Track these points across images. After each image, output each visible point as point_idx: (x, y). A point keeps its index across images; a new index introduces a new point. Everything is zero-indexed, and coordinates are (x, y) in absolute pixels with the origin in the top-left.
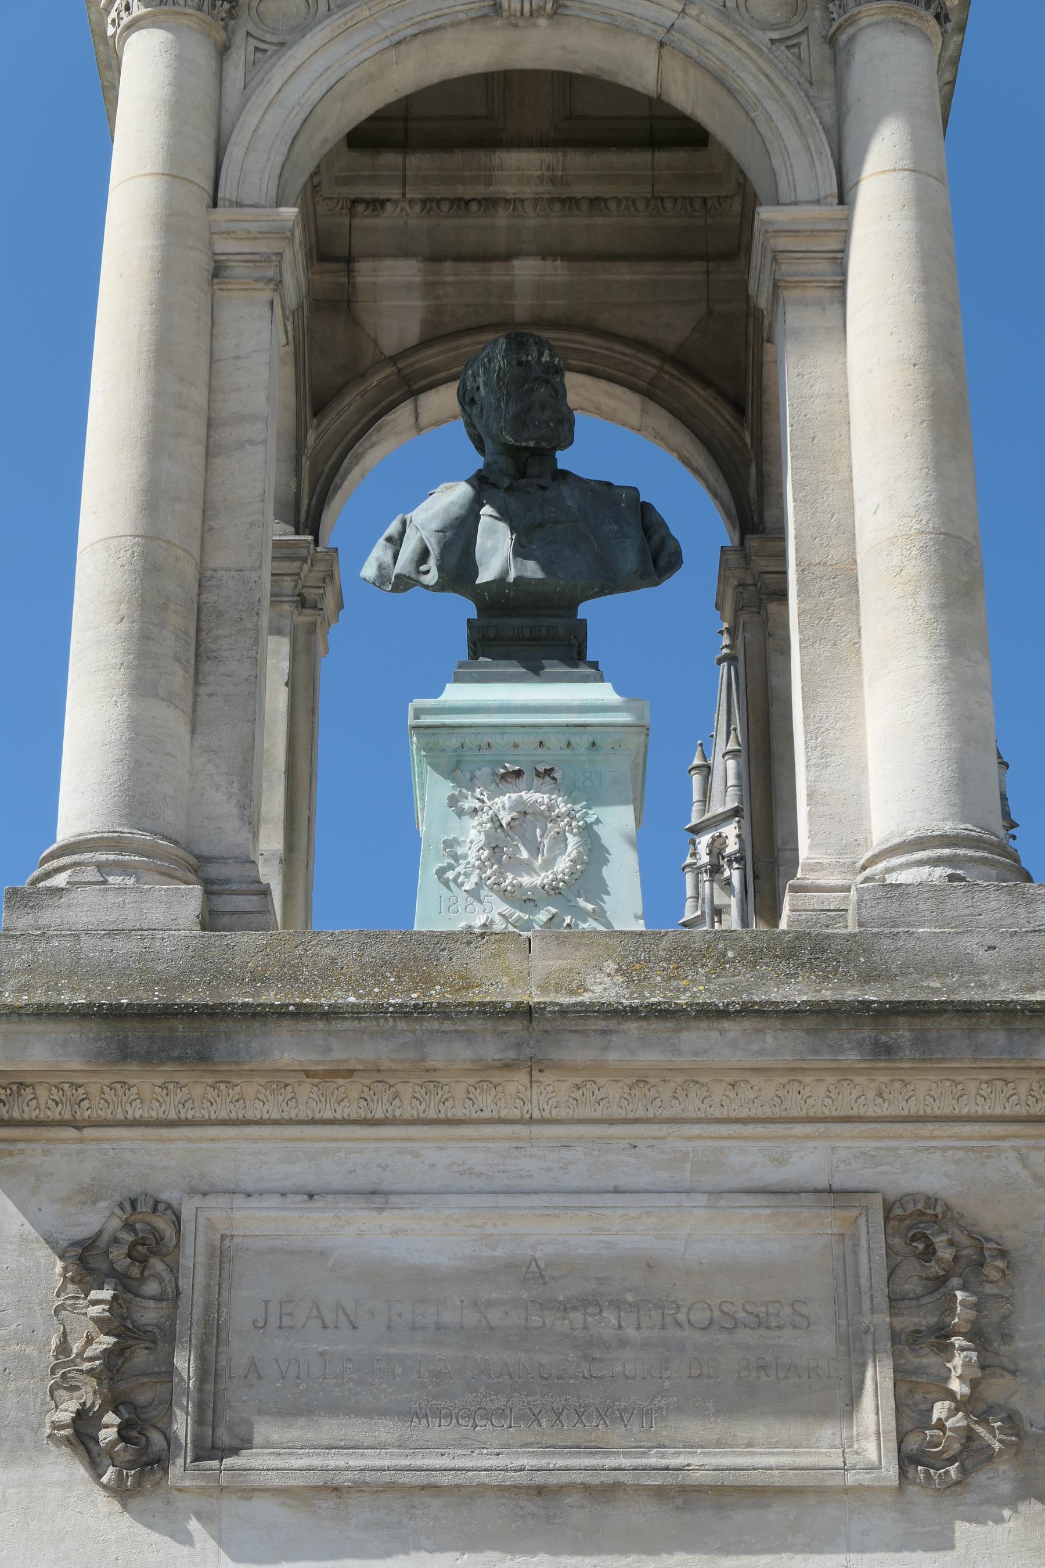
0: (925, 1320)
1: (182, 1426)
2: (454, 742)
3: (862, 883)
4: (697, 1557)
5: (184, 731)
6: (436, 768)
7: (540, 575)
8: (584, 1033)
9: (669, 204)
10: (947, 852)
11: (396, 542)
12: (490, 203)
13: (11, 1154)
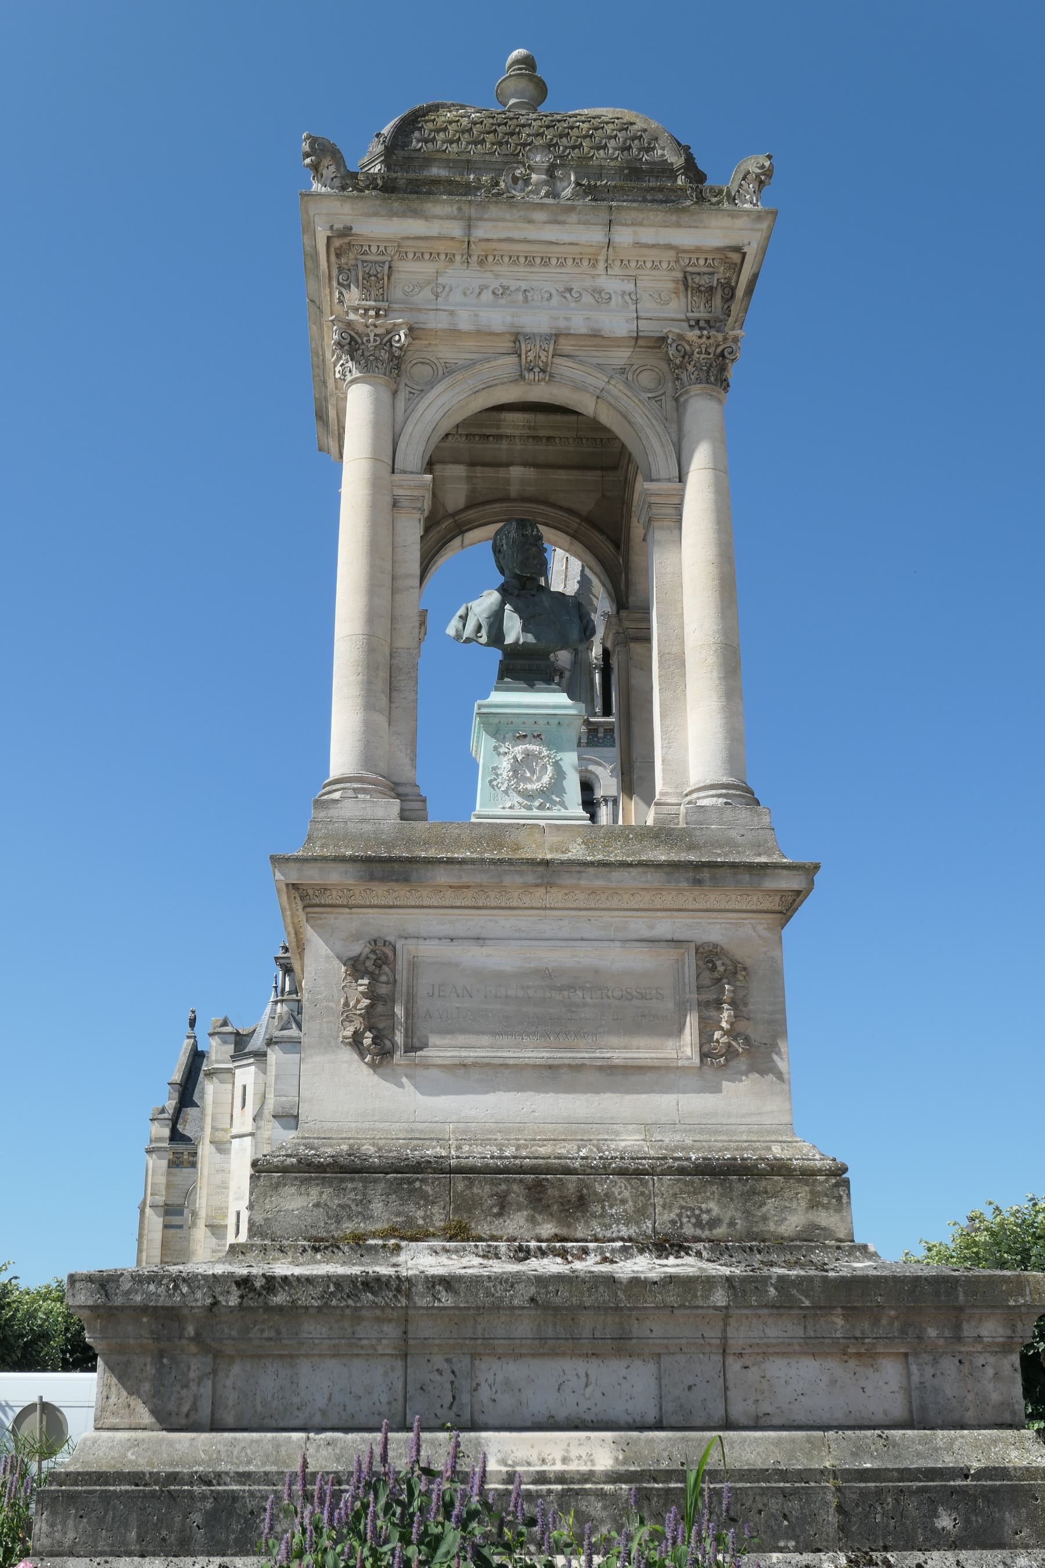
0: (711, 996)
1: (399, 1038)
2: (496, 720)
3: (688, 804)
4: (616, 1095)
5: (386, 725)
6: (487, 732)
7: (534, 641)
8: (570, 872)
9: (584, 441)
10: (724, 791)
11: (464, 618)
12: (499, 437)
13: (321, 919)
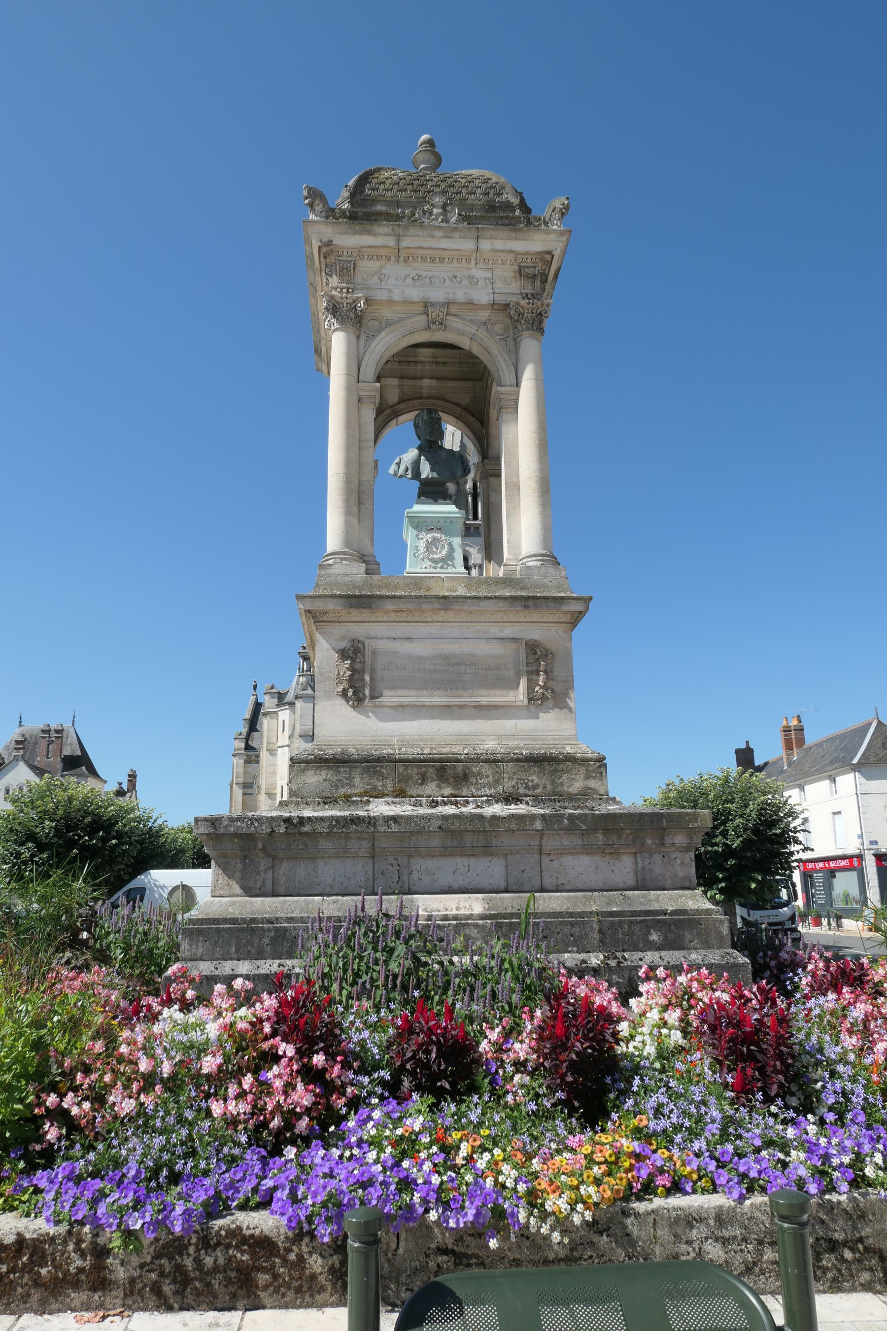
1: (367, 692)
11: (399, 464)
12: (416, 362)
